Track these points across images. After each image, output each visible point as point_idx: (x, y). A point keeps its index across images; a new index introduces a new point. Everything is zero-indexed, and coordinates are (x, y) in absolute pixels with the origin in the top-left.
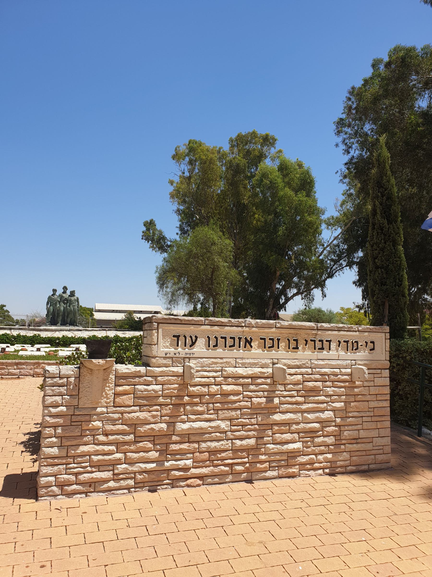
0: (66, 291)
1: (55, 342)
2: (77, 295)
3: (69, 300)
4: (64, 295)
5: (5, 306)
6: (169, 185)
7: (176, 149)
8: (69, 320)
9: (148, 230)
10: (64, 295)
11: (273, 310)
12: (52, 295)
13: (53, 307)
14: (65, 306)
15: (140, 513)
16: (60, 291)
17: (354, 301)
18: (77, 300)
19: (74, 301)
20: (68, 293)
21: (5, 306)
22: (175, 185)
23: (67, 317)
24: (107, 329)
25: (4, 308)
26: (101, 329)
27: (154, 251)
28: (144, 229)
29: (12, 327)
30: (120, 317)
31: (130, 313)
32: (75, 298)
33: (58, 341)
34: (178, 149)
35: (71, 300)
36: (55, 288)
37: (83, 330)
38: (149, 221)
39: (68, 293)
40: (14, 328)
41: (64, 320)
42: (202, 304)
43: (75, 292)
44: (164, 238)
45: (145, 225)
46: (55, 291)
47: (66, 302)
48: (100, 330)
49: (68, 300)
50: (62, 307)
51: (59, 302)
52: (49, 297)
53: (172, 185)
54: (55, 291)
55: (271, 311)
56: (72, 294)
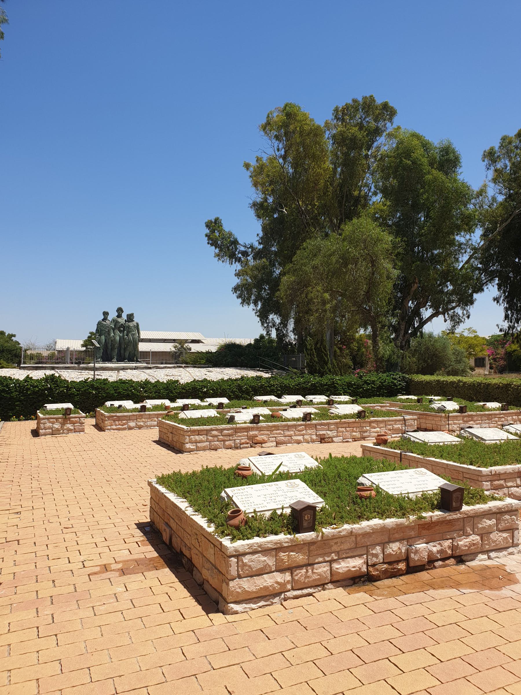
0: (121, 314)
1: (201, 391)
2: (136, 320)
3: (127, 327)
4: (119, 320)
5: (14, 336)
6: (244, 169)
7: (268, 117)
8: (127, 354)
9: (213, 231)
10: (119, 320)
11: (405, 336)
12: (103, 320)
13: (106, 337)
14: (121, 335)
15: (159, 581)
16: (113, 315)
17: (498, 324)
18: (137, 327)
19: (133, 328)
20: (124, 316)
21: (14, 336)
22: (252, 169)
23: (125, 349)
24: (183, 365)
25: (13, 338)
26: (176, 365)
27: (220, 262)
28: (207, 231)
29: (55, 365)
30: (169, 347)
31: (182, 342)
32: (134, 323)
33: (205, 390)
34: (270, 116)
35: (129, 327)
36: (106, 310)
37: (154, 367)
38: (213, 221)
39: (124, 316)
40: (58, 367)
41: (120, 354)
42: (277, 330)
43: (134, 315)
44: (235, 242)
45: (207, 226)
46: (106, 314)
47: (122, 329)
48: (174, 367)
49: (124, 327)
50: (117, 336)
51: (114, 330)
52: (99, 324)
53: (248, 169)
54: (106, 314)
55: (402, 338)
56: (130, 318)
